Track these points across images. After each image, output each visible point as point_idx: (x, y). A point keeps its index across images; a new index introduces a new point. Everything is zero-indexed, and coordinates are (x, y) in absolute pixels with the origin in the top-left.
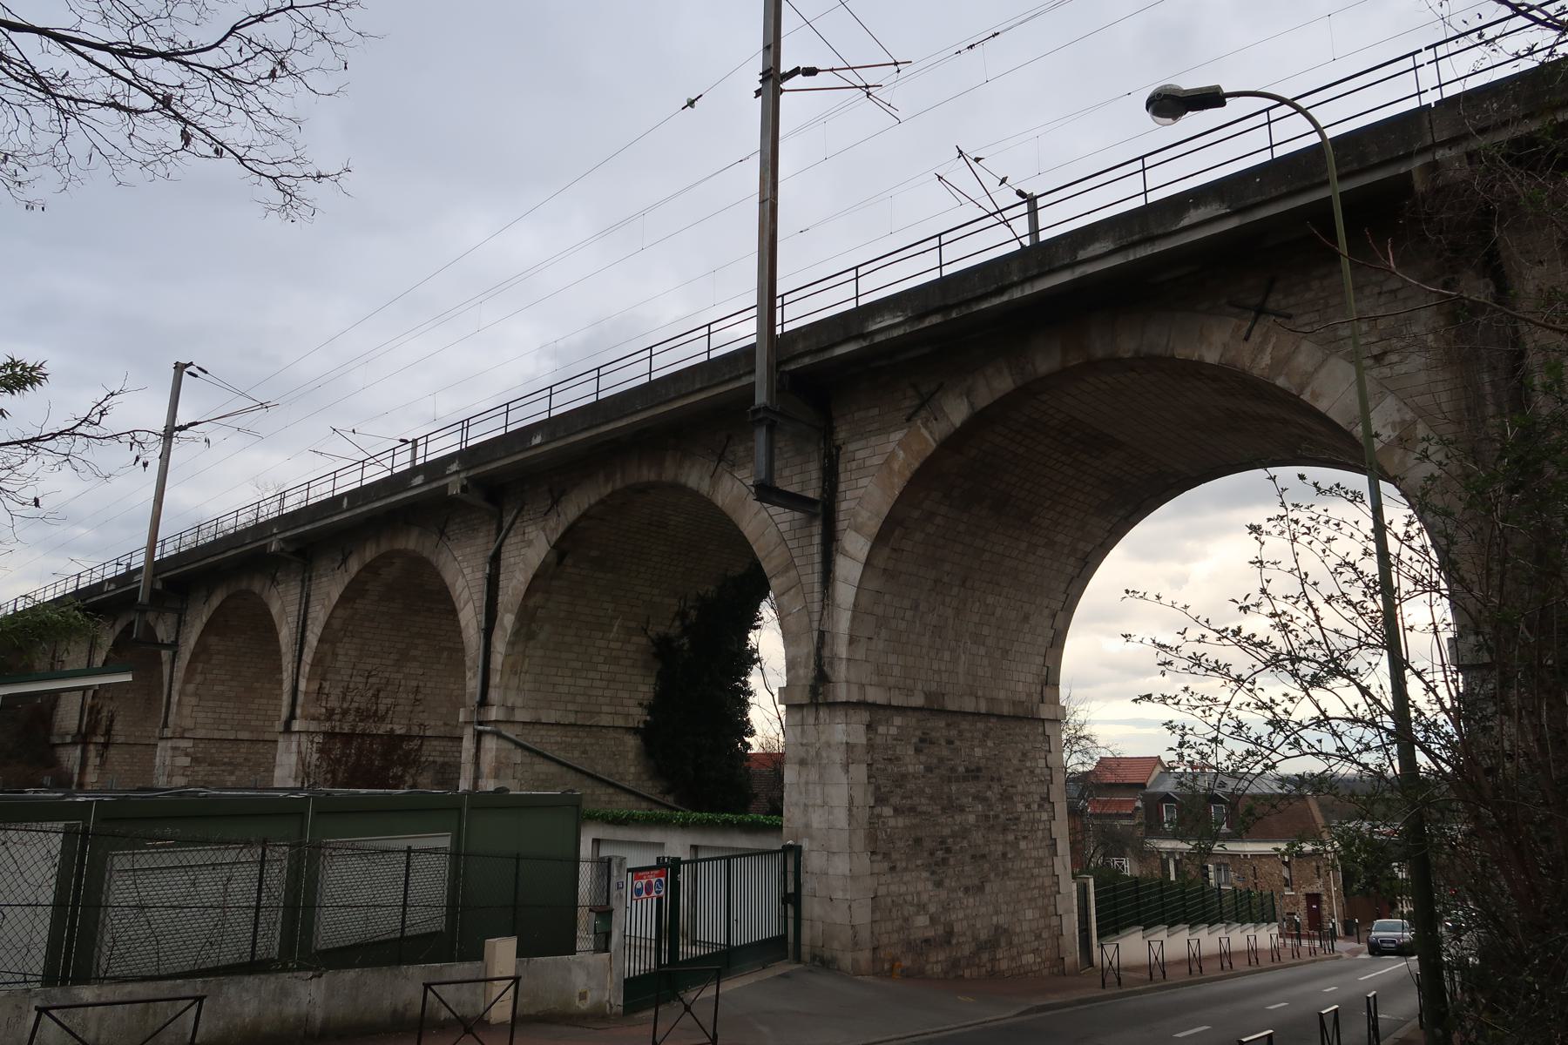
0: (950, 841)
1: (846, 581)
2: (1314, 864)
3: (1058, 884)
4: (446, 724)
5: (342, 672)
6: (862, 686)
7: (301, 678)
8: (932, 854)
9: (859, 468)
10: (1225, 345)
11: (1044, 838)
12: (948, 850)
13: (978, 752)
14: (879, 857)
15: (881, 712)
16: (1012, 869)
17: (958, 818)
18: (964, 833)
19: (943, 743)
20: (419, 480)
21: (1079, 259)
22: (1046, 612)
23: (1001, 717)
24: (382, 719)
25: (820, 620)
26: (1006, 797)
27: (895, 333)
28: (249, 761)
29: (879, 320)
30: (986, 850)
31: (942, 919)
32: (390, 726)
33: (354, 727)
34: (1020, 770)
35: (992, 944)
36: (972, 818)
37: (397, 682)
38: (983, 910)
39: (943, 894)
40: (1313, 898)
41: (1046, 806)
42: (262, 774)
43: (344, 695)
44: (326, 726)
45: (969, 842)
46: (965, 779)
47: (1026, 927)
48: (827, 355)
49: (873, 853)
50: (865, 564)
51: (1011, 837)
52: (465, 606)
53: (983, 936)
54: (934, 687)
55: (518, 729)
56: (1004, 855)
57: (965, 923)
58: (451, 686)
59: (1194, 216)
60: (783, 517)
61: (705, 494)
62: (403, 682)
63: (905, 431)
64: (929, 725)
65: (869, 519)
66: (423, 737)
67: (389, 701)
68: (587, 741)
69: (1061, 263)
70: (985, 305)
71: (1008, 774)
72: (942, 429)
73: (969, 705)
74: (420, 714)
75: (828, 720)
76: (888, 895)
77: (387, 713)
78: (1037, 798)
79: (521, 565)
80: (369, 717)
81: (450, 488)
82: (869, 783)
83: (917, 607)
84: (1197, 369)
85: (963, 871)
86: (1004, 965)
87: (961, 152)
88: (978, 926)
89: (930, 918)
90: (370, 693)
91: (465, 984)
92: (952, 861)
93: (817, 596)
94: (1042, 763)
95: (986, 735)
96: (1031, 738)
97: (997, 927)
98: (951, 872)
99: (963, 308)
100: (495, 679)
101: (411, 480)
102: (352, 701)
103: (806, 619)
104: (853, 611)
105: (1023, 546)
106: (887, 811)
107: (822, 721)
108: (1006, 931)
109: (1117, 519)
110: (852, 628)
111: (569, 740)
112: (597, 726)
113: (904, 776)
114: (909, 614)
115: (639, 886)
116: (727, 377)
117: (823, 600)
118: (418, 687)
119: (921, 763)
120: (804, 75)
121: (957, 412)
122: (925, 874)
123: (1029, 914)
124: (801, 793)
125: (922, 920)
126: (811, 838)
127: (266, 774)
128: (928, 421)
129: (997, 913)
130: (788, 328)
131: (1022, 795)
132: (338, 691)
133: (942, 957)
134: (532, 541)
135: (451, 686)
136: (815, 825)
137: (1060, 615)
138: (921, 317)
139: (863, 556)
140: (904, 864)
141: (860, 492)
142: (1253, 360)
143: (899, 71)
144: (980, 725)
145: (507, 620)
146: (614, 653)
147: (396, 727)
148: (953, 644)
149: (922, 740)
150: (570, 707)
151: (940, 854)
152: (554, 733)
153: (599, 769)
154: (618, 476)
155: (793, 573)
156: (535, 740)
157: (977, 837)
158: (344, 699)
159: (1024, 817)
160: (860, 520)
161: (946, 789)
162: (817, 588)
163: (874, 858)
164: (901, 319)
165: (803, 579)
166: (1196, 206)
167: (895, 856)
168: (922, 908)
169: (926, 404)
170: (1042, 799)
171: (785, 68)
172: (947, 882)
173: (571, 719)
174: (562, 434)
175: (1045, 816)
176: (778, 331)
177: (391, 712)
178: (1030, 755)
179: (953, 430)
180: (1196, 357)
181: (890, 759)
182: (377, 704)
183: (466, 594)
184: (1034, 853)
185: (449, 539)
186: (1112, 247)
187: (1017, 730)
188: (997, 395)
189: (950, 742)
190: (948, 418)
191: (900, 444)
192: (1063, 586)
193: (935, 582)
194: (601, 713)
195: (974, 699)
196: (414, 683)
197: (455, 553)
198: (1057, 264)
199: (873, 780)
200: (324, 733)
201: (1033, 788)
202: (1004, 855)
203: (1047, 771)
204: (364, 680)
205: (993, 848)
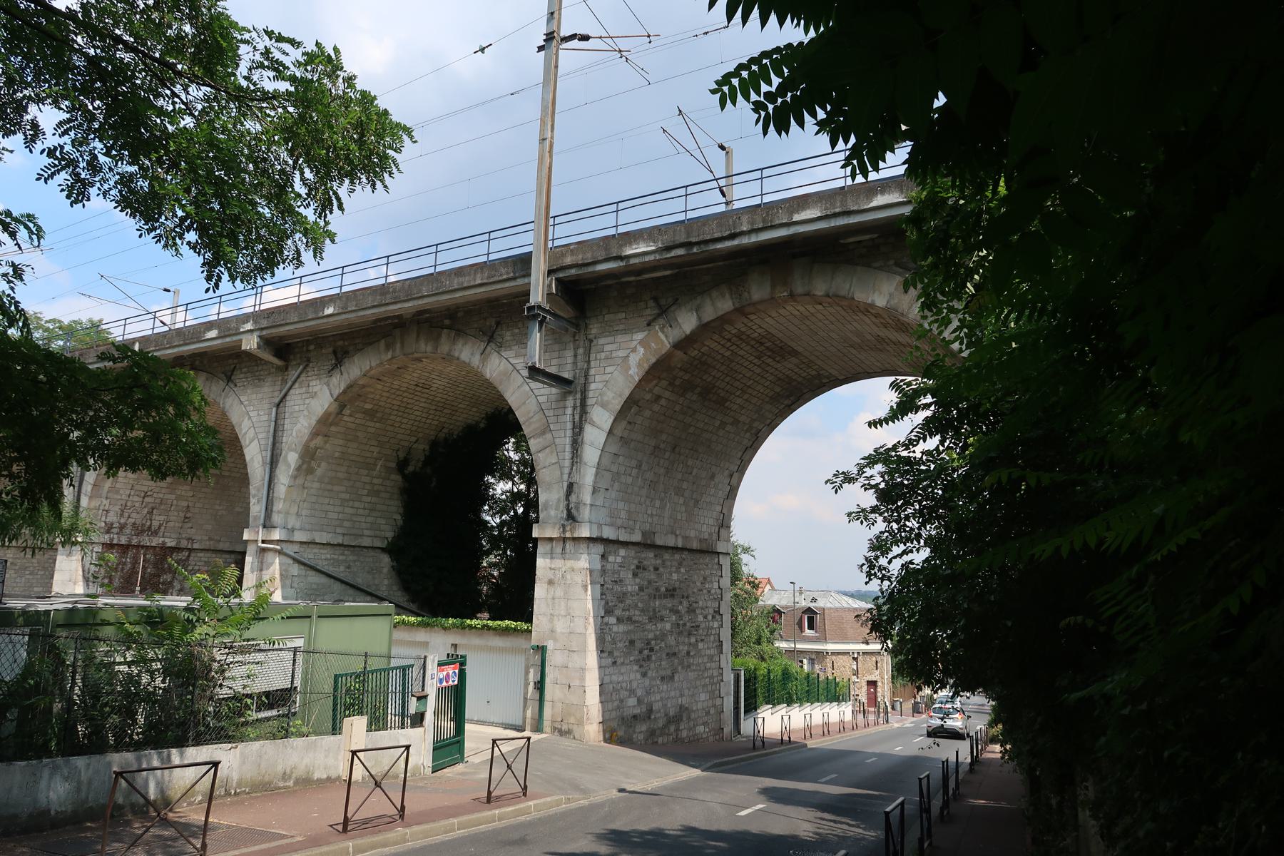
0: (653, 642)
1: (592, 445)
2: (874, 659)
3: (722, 674)
4: (210, 539)
5: (121, 492)
6: (600, 525)
7: (82, 496)
8: (641, 652)
9: (606, 358)
10: (891, 295)
11: (714, 641)
12: (652, 650)
13: (675, 576)
14: (605, 655)
15: (611, 545)
16: (693, 664)
17: (659, 626)
18: (662, 637)
19: (652, 570)
20: (213, 334)
21: (794, 220)
22: (726, 473)
23: (691, 551)
24: (156, 533)
25: (570, 474)
26: (691, 610)
27: (647, 259)
28: (16, 565)
29: (634, 247)
30: (676, 650)
31: (646, 701)
32: (163, 539)
33: (130, 540)
34: (702, 590)
35: (676, 719)
36: (668, 626)
37: (169, 502)
38: (672, 694)
39: (647, 682)
40: (872, 684)
41: (718, 617)
42: (28, 577)
43: (123, 511)
44: (106, 538)
45: (666, 643)
46: (665, 597)
47: (700, 706)
48: (591, 269)
49: (602, 651)
50: (609, 433)
51: (693, 640)
52: (250, 443)
53: (672, 713)
54: (647, 527)
55: (296, 548)
56: (688, 653)
57: (660, 703)
58: (217, 507)
59: (880, 200)
60: (544, 392)
61: (476, 367)
62: (175, 502)
63: (645, 333)
64: (643, 556)
65: (613, 398)
66: (191, 550)
67: (162, 518)
68: (351, 558)
69: (780, 222)
70: (719, 246)
71: (694, 593)
72: (675, 334)
73: (671, 542)
74: (189, 530)
75: (572, 552)
76: (611, 682)
77: (159, 528)
78: (711, 611)
79: (306, 413)
80: (143, 531)
81: (243, 344)
82: (601, 599)
83: (640, 466)
84: (868, 309)
85: (661, 665)
86: (684, 734)
87: (680, 111)
88: (669, 705)
89: (638, 700)
90: (146, 510)
91: (363, 748)
92: (653, 658)
93: (568, 455)
94: (716, 585)
95: (680, 564)
96: (710, 566)
97: (681, 706)
98: (652, 665)
99: (702, 246)
100: (279, 506)
101: (205, 333)
102: (129, 517)
103: (558, 473)
104: (597, 468)
105: (717, 423)
106: (613, 620)
107: (568, 551)
108: (687, 709)
109: (783, 406)
110: (595, 482)
111: (336, 557)
112: (359, 547)
113: (625, 594)
114: (635, 471)
115: (441, 677)
116: (505, 277)
117: (572, 459)
118: (188, 506)
119: (636, 584)
120: (579, 40)
121: (687, 322)
122: (636, 668)
123: (703, 697)
124: (548, 606)
125: (632, 702)
126: (555, 640)
127: (31, 577)
128: (664, 326)
129: (682, 696)
130: (557, 243)
131: (702, 608)
132: (117, 508)
133: (644, 728)
134: (316, 393)
135: (217, 507)
136: (559, 630)
137: (736, 475)
138: (668, 249)
139: (607, 426)
140: (622, 660)
141: (607, 377)
142: (910, 308)
143: (650, 42)
144: (677, 556)
145: (291, 458)
146: (376, 488)
147: (167, 540)
148: (663, 494)
149: (638, 567)
150: (339, 530)
151: (646, 652)
152: (326, 551)
153: (360, 581)
154: (398, 345)
155: (549, 436)
156: (310, 557)
157: (671, 640)
158: (122, 515)
159: (703, 626)
160: (606, 398)
161: (652, 604)
162: (568, 448)
163: (604, 655)
164: (653, 248)
165: (557, 441)
166: (882, 192)
167: (616, 654)
168: (632, 692)
169: (664, 313)
170: (715, 612)
171: (565, 32)
172: (650, 673)
173: (339, 540)
174: (354, 308)
175: (716, 625)
176: (550, 244)
177: (163, 528)
178: (709, 579)
179: (683, 336)
180: (869, 301)
181: (616, 581)
182: (151, 520)
183: (251, 433)
184: (708, 652)
185: (236, 385)
186: (819, 215)
187: (701, 561)
188: (720, 313)
189: (656, 569)
190: (681, 327)
191: (641, 342)
192: (740, 454)
193: (655, 447)
194: (363, 535)
195: (674, 536)
196: (184, 503)
197: (241, 397)
198: (777, 222)
199: (604, 597)
200: (103, 544)
201: (709, 603)
202: (688, 653)
203: (719, 591)
204: (141, 499)
205: (681, 648)
